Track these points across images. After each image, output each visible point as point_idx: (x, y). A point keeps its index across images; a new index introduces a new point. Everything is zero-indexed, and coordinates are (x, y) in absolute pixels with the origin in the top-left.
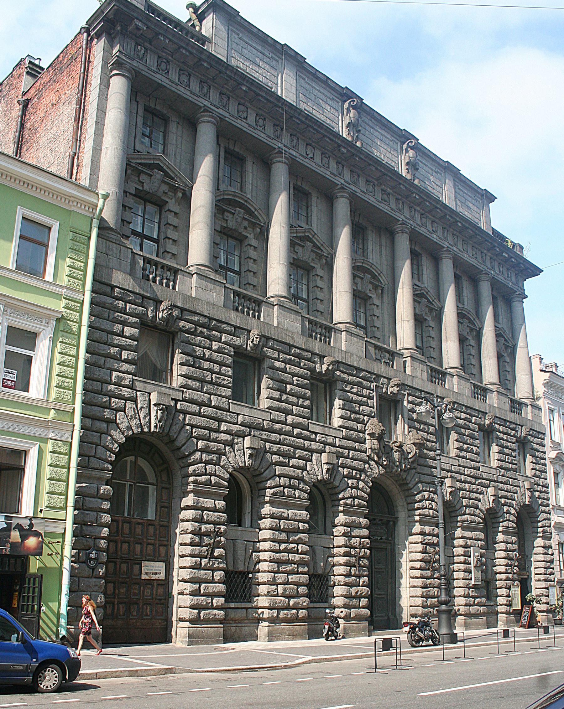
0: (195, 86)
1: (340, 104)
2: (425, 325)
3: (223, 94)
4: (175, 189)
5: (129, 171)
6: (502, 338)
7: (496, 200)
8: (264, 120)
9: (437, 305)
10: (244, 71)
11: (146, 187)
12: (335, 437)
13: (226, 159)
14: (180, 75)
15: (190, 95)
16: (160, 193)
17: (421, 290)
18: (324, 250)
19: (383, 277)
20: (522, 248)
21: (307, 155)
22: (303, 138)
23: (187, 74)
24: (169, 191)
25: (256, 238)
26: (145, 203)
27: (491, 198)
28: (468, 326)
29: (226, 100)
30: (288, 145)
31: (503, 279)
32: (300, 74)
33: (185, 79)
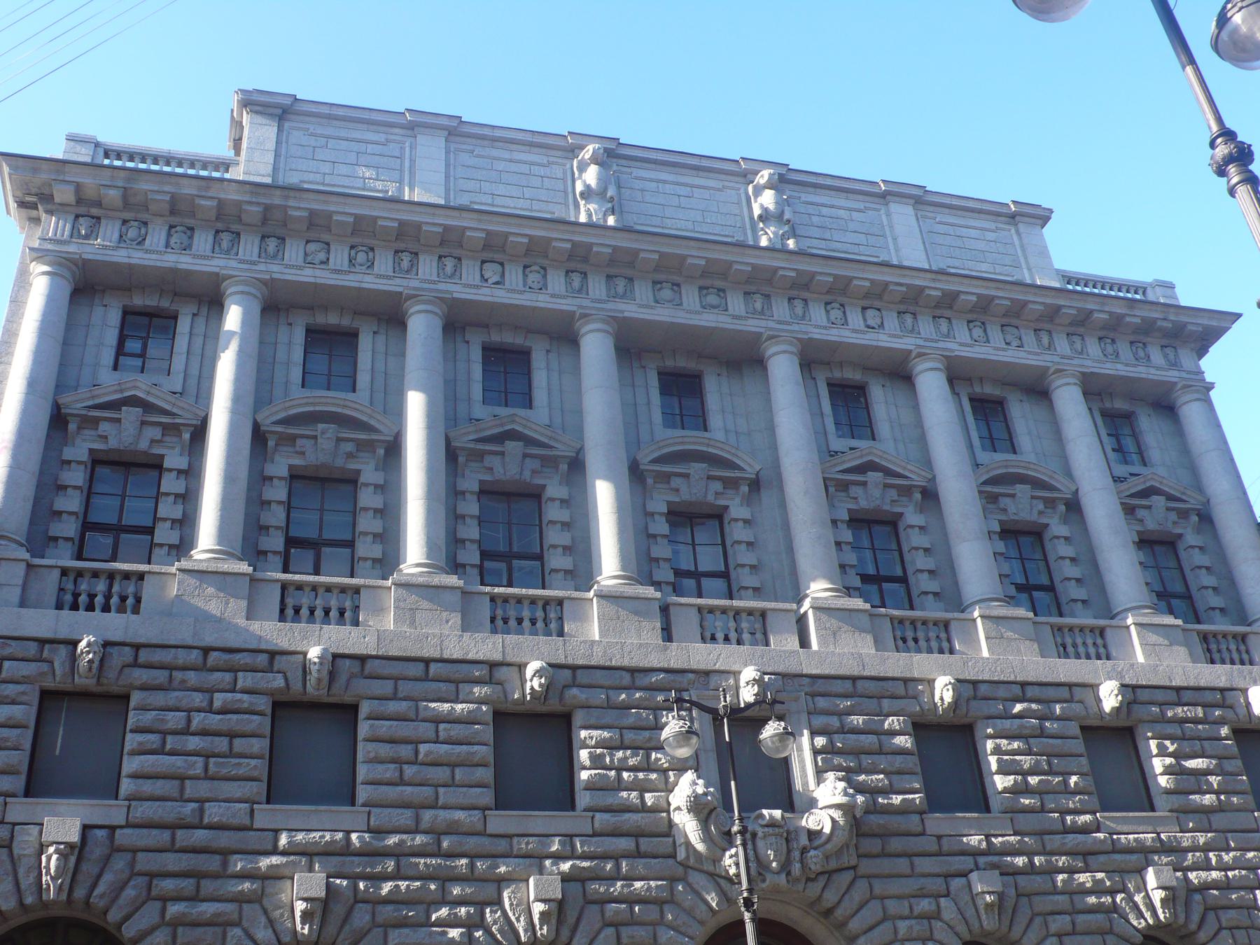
0: (855, 319)
1: (1013, 231)
2: (1181, 547)
3: (572, 272)
4: (906, 491)
5: (832, 490)
6: (1155, 498)
7: (1053, 215)
8: (1113, 341)
9: (919, 475)
10: (691, 231)
11: (863, 504)
12: (571, 836)
13: (975, 410)
14: (970, 330)
15: (889, 339)
16: (711, 498)
17: (1145, 482)
18: (556, 445)
19: (745, 457)
20: (1171, 286)
21: (486, 280)
22: (815, 296)
23: (838, 306)
24: (1046, 507)
25: (1065, 520)
26: (691, 521)
27: (1041, 217)
28: (1168, 509)
29: (579, 279)
30: (934, 336)
31: (549, 299)
32: (924, 213)
33: (836, 314)
